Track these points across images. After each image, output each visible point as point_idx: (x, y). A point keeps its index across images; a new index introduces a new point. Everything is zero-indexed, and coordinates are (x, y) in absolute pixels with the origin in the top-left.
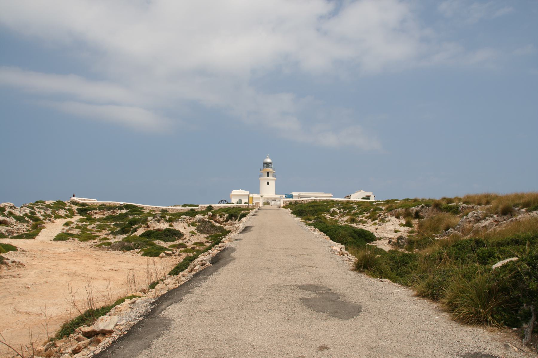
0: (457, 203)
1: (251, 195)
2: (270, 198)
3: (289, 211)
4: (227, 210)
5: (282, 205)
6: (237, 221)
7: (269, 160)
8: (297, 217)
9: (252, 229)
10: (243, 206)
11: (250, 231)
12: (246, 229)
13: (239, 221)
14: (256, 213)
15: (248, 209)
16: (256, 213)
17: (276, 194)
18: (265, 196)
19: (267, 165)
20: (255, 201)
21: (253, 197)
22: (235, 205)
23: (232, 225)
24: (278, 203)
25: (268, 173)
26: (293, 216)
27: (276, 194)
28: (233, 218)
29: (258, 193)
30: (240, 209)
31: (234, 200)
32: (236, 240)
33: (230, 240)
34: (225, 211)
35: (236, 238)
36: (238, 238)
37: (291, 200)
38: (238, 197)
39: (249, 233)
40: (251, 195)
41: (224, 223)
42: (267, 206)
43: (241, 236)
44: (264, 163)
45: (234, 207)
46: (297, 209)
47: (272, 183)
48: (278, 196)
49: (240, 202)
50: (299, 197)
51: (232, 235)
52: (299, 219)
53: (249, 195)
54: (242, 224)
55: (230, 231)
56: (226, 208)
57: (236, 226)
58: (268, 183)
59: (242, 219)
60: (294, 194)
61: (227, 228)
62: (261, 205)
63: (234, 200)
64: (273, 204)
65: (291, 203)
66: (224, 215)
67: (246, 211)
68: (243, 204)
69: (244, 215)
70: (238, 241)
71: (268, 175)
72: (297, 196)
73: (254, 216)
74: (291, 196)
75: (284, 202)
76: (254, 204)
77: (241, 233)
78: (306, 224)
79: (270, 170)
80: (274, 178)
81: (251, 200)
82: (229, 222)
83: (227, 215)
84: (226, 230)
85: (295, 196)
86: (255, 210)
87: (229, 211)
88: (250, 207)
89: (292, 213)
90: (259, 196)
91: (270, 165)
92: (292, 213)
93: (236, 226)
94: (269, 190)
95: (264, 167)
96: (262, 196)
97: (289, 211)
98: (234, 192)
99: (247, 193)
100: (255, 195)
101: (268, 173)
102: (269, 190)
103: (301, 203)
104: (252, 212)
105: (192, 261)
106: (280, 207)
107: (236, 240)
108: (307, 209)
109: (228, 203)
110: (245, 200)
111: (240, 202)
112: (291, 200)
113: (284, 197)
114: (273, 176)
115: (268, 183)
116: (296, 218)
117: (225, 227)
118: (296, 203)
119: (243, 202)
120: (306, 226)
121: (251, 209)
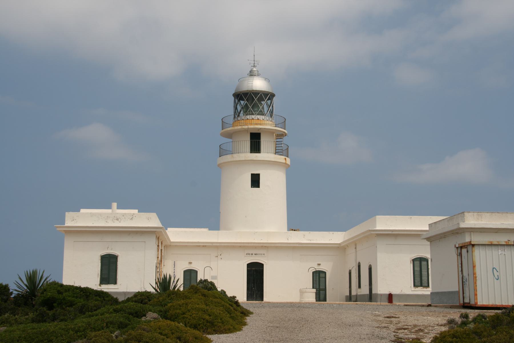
47: (274, 181)
58: (255, 181)
79: (262, 123)
80: (281, 159)
95: (237, 114)
99: (152, 221)
111: (109, 266)
115: (255, 181)
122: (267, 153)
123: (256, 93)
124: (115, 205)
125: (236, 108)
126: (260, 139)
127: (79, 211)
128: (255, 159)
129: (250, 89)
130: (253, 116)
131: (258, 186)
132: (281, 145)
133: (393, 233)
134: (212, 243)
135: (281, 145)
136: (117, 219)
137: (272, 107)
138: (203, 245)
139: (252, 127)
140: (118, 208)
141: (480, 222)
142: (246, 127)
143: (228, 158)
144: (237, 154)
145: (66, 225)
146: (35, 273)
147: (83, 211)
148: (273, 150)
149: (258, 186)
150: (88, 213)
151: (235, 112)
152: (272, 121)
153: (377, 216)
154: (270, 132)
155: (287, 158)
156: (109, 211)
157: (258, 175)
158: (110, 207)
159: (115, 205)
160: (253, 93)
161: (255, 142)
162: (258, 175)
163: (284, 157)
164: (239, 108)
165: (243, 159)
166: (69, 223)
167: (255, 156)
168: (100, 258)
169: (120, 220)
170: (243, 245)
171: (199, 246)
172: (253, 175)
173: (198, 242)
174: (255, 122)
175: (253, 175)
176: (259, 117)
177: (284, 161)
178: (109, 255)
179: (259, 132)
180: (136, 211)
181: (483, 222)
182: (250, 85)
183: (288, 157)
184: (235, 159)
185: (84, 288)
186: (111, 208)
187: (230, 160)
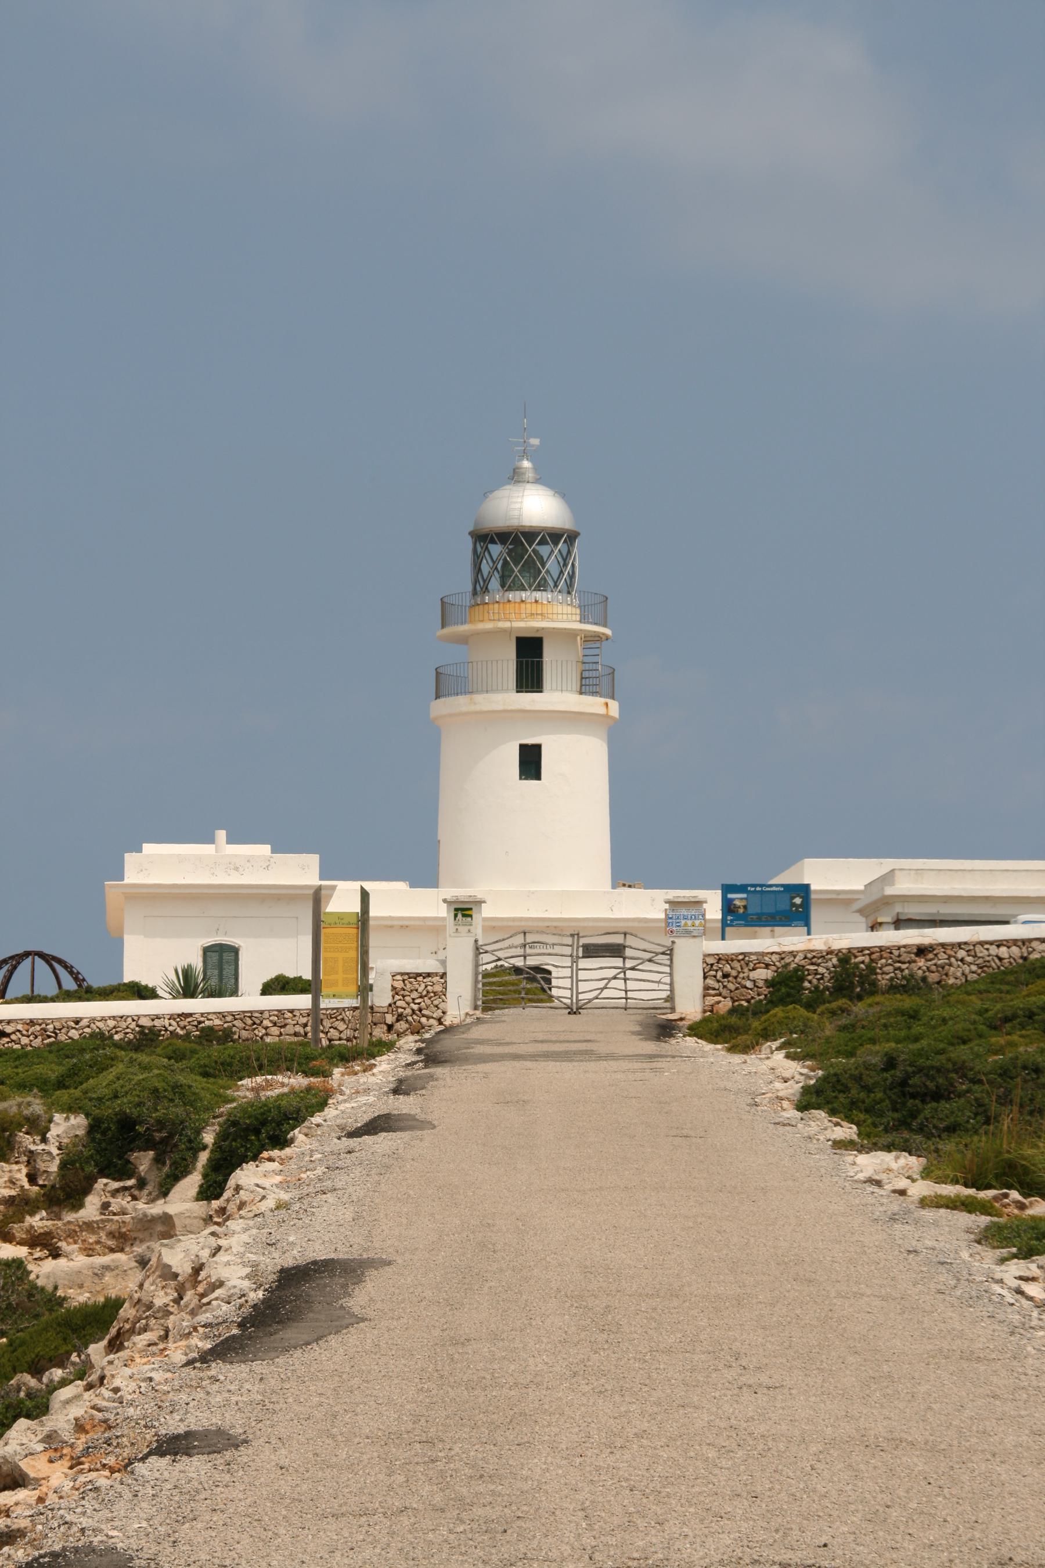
0: (868, 1097)
1: (343, 899)
2: (554, 928)
3: (777, 1071)
4: (69, 1066)
5: (690, 1006)
6: (183, 1200)
7: (535, 506)
8: (868, 1142)
9: (360, 1298)
10: (253, 1018)
11: (344, 1321)
12: (292, 1302)
13: (211, 1190)
14: (404, 1105)
15: (318, 1054)
16: (404, 1105)
17: (624, 876)
18: (504, 902)
19: (515, 555)
20: (387, 963)
21: (363, 919)
22: (166, 1006)
23: (122, 1240)
24: (646, 987)
25: (530, 653)
26: (828, 1128)
27: (624, 876)
28: (144, 1161)
29: (424, 873)
30: (222, 1051)
31: (154, 956)
32: (174, 1446)
33: (93, 1448)
34: (45, 1087)
35: (173, 1425)
36: (197, 1420)
37: (790, 941)
38: (197, 912)
39: (331, 1354)
40: (343, 899)
41: (38, 1221)
42: (519, 1023)
43: (231, 1394)
44: (483, 538)
45: (147, 1038)
46: (873, 1055)
47: (580, 764)
48: (646, 905)
49: (219, 969)
50: (876, 909)
51: (134, 1377)
52: (896, 1166)
53: (318, 898)
54: (239, 1234)
55: (99, 1321)
56: (59, 1050)
57: (177, 1256)
58: (530, 761)
59: (246, 1176)
60: (823, 875)
61: (70, 1273)
62: (459, 1002)
63: (154, 956)
64: (587, 990)
65: (788, 982)
66: (39, 1128)
67: (289, 1082)
68: (249, 999)
69: (263, 1132)
70: (195, 1467)
71: (530, 672)
72: (856, 895)
73: (381, 1143)
74: (794, 906)
75: (717, 968)
76: (381, 998)
77: (224, 1350)
78: (991, 1237)
79: (552, 613)
80: (594, 704)
81: (340, 954)
82: (91, 1209)
83: (66, 1127)
84: (54, 1301)
85: (840, 901)
86: (385, 1068)
87: (101, 1084)
88: (338, 1033)
89: (809, 1100)
90: (429, 904)
91: (551, 556)
92: (809, 1100)
93: (177, 1256)
94: (540, 840)
95: (480, 587)
96: (463, 911)
97: (777, 1071)
98: (158, 864)
99: (301, 871)
100: (393, 900)
101: (530, 653)
102: (540, 840)
103: (909, 986)
104: (358, 1092)
105: (348, 1061)
106: (665, 1030)
107: (174, 1446)
108: (989, 1054)
109: (86, 993)
110: (274, 951)
111: (219, 969)
112: (790, 941)
113: (714, 910)
114: (587, 685)
115: (530, 761)
116: (870, 1163)
117: (45, 1271)
118: (852, 975)
119: (252, 973)
120: (985, 1260)
121: (345, 1057)
122: (558, 695)
123: (531, 535)
124: (221, 835)
125: (477, 570)
126: (541, 655)
127: (140, 850)
128: (528, 708)
129: (515, 523)
130: (524, 595)
131: (538, 776)
132: (594, 666)
133: (840, 897)
134: (425, 919)
135: (594, 666)
136: (237, 869)
137: (573, 565)
138: (401, 923)
139: (521, 624)
140: (230, 841)
141: (920, 886)
142: (507, 625)
143: (459, 703)
144: (485, 695)
145: (126, 881)
146: (190, 966)
147: (148, 848)
148: (576, 685)
149: (538, 776)
150: (171, 856)
151: (476, 582)
152: (571, 604)
153: (807, 861)
154: (570, 635)
155: (610, 702)
156: (207, 849)
157: (538, 748)
158: (211, 840)
159: (221, 835)
160: (522, 533)
161: (529, 660)
162: (538, 748)
163: (603, 700)
164: (485, 568)
165: (500, 708)
166: (131, 877)
167: (529, 700)
168: (201, 953)
169: (241, 869)
170: (499, 924)
171: (391, 927)
172: (523, 748)
173: (391, 918)
174: (529, 608)
175: (523, 748)
176: (538, 595)
177: (602, 711)
178: (221, 945)
179: (538, 635)
180: (265, 849)
181: (924, 886)
182: (516, 513)
183: (613, 698)
184: (478, 708)
185: (295, 978)
186: (213, 843)
187: (464, 709)
